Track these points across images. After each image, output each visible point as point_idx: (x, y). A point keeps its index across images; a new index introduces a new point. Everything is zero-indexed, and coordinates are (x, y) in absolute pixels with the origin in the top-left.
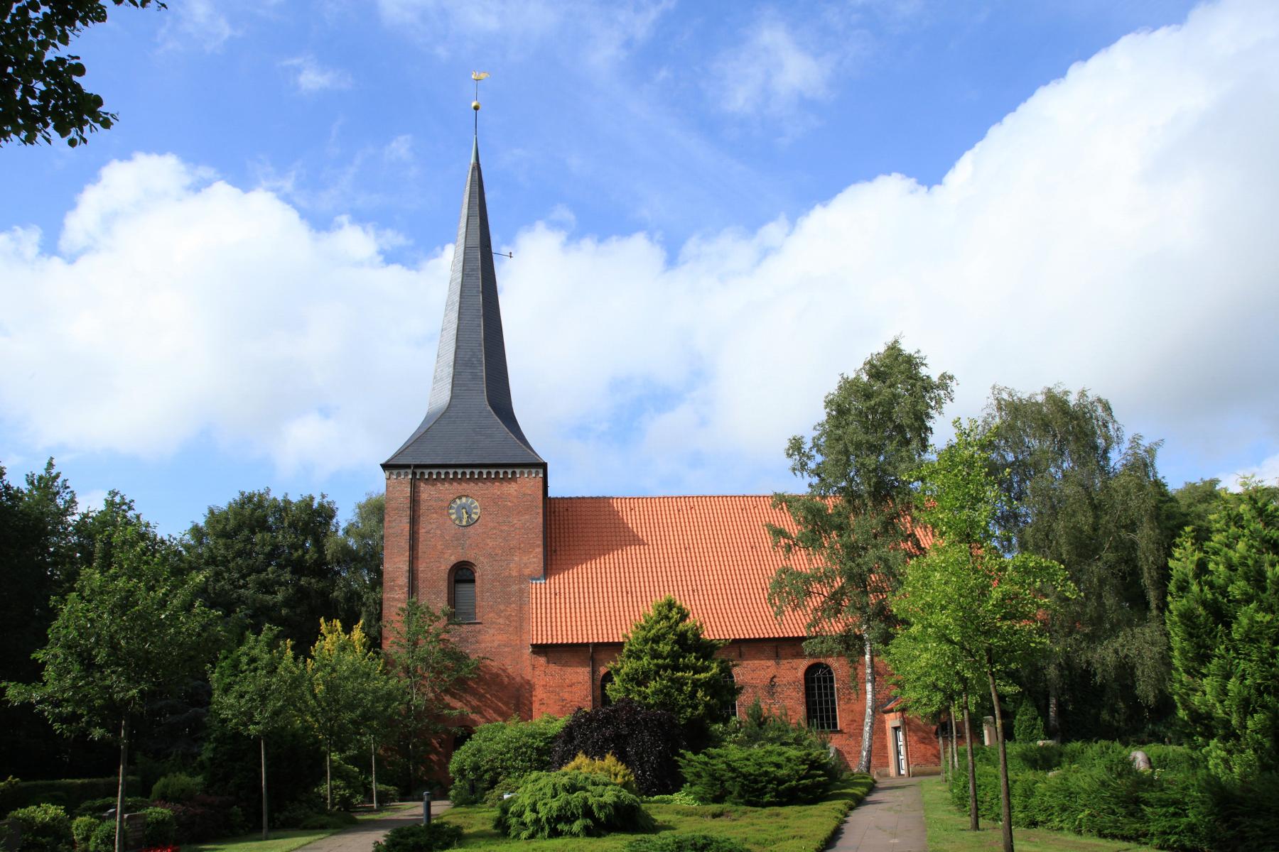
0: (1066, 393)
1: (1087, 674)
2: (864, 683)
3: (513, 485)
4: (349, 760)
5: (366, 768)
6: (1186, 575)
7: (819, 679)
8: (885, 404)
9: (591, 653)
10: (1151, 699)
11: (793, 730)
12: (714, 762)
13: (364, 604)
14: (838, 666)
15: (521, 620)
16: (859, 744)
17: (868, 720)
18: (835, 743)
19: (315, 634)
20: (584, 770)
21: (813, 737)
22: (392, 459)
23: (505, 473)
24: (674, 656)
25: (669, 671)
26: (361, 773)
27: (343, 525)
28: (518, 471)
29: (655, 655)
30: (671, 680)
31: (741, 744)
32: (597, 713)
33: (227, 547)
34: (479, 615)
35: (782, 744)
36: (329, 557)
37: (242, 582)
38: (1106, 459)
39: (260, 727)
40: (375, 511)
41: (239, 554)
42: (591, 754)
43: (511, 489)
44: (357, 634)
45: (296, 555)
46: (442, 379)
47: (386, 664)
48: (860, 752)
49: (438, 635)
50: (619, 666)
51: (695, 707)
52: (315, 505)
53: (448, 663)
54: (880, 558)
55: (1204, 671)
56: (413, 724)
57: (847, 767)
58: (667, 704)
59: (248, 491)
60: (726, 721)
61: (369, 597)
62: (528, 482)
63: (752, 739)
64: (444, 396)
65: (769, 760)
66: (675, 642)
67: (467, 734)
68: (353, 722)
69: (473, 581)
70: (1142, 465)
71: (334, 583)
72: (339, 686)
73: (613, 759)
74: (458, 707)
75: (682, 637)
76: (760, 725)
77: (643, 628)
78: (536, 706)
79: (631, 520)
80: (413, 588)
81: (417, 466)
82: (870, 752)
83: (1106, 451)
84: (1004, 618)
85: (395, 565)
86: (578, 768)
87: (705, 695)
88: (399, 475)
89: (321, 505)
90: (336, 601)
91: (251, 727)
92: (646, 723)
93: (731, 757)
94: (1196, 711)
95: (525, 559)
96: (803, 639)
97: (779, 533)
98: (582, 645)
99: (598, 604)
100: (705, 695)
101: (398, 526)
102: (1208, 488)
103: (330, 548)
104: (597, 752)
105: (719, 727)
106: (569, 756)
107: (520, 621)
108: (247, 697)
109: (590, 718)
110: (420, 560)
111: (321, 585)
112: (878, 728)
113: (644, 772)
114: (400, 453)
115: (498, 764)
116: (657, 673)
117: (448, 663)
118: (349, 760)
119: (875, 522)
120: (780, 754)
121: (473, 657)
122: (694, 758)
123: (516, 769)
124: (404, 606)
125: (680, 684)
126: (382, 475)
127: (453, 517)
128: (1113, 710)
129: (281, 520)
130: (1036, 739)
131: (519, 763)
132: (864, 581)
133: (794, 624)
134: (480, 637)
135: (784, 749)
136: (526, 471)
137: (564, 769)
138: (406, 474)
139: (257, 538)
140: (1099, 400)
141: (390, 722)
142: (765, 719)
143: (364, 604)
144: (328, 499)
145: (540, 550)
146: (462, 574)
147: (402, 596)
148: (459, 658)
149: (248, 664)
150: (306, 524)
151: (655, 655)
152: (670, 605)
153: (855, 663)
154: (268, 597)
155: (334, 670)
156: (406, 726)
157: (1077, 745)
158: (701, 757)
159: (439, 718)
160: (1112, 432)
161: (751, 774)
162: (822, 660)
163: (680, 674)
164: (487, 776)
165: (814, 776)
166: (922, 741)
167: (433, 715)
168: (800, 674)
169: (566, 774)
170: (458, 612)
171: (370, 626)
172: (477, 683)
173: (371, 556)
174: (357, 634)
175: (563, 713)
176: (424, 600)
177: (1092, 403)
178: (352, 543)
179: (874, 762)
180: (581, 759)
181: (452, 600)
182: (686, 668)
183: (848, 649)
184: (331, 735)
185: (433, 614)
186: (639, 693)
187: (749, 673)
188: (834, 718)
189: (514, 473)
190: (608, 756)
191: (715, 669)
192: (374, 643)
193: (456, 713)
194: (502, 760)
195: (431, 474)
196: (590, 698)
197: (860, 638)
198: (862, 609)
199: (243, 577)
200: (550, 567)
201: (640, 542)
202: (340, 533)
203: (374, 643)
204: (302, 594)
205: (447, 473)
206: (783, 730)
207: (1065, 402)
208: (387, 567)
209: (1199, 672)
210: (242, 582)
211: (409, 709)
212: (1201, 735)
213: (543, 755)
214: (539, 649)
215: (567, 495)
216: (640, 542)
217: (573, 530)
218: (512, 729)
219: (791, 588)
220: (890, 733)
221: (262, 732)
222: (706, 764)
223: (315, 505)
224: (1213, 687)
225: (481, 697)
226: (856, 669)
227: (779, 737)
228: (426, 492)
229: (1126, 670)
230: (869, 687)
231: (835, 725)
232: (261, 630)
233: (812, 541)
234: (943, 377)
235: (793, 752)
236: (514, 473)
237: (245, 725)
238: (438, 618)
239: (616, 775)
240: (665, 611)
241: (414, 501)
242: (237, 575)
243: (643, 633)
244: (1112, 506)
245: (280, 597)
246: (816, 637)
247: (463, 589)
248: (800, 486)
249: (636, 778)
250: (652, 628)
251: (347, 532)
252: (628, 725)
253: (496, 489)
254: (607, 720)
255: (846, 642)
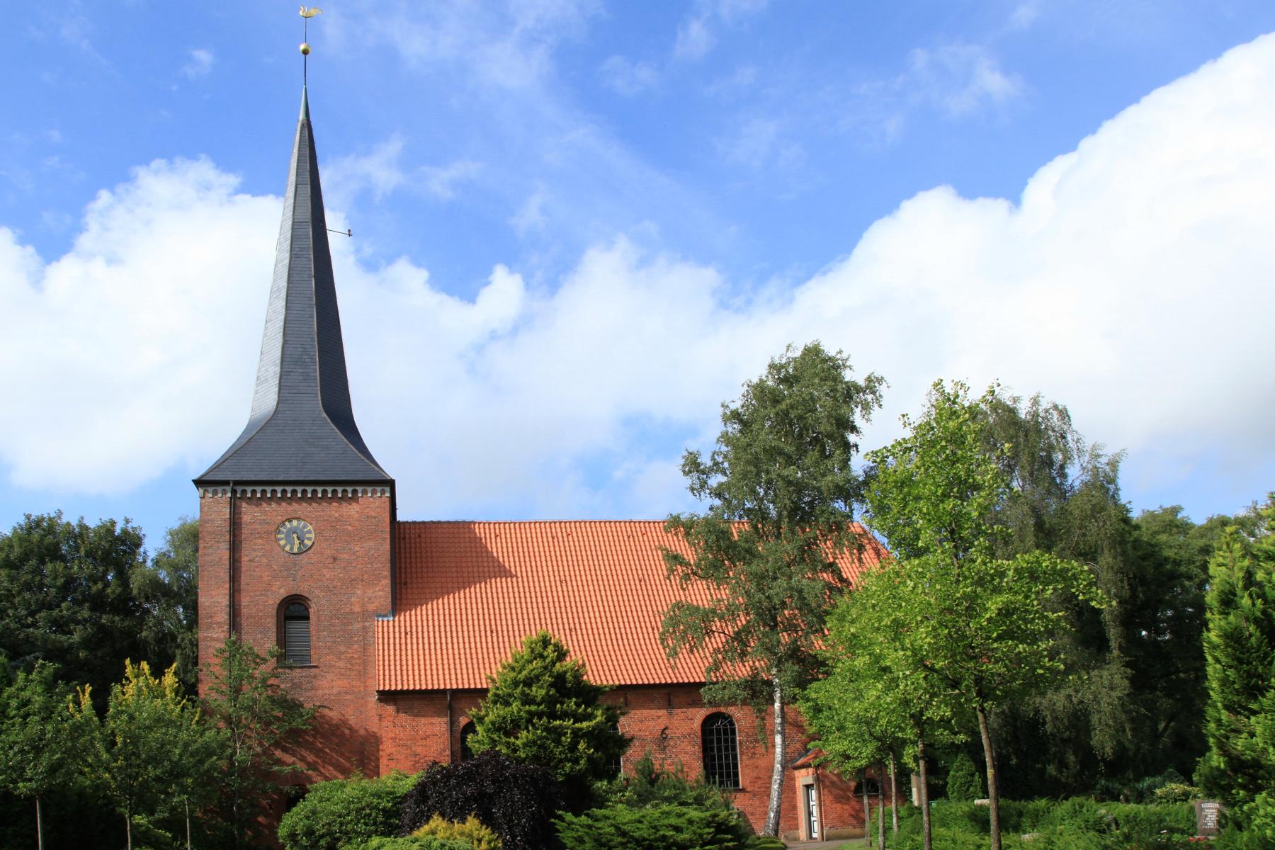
0: (1015, 400)
1: (1036, 723)
2: (773, 734)
3: (355, 506)
4: (160, 824)
5: (179, 833)
6: (1232, 585)
7: (718, 731)
8: (801, 413)
9: (447, 701)
10: (1108, 750)
11: (692, 788)
12: (599, 825)
13: (178, 646)
14: (742, 717)
15: (365, 664)
16: (765, 805)
17: (776, 777)
18: (739, 803)
19: (120, 677)
20: (440, 835)
21: (716, 795)
22: (206, 474)
23: (345, 491)
24: (550, 701)
25: (545, 719)
26: (175, 838)
27: (152, 554)
28: (360, 489)
29: (527, 700)
30: (547, 729)
31: (629, 803)
32: (456, 767)
33: (12, 579)
34: (314, 657)
35: (681, 804)
36: (135, 592)
37: (30, 620)
38: (1064, 476)
39: (34, 785)
40: (189, 537)
41: (28, 587)
42: (448, 816)
43: (352, 510)
44: (169, 679)
45: (94, 589)
46: (266, 380)
47: (204, 713)
48: (766, 813)
49: (264, 681)
50: (483, 713)
51: (576, 761)
52: (118, 531)
53: (278, 713)
54: (792, 589)
55: (1254, 707)
56: (235, 782)
57: (752, 831)
58: (542, 757)
59: (36, 513)
60: (612, 776)
61: (183, 637)
62: (373, 502)
63: (642, 799)
64: (270, 400)
65: (666, 822)
66: (552, 685)
67: (301, 795)
68: (158, 779)
69: (307, 618)
70: (1103, 485)
71: (142, 620)
72: (139, 737)
73: (476, 822)
74: (290, 763)
75: (559, 680)
76: (652, 782)
77: (513, 669)
78: (383, 762)
79: (497, 549)
80: (234, 622)
81: (237, 483)
82: (778, 813)
83: (1062, 467)
84: (1000, 638)
85: (213, 599)
86: (433, 833)
87: (588, 748)
88: (215, 493)
89: (125, 531)
90: (145, 641)
91: (21, 785)
92: (516, 779)
93: (619, 819)
94: (1238, 758)
95: (369, 593)
96: (702, 685)
97: (675, 559)
98: (438, 691)
99: (462, 643)
100: (588, 748)
101: (216, 553)
102: (1168, 518)
103: (136, 583)
104: (456, 813)
105: (602, 785)
106: (421, 818)
107: (363, 666)
108: (16, 749)
109: (447, 774)
110: (243, 594)
111: (126, 623)
112: (787, 786)
113: (514, 837)
114: (218, 466)
115: (336, 828)
116: (529, 721)
117: (278, 713)
118: (160, 824)
119: (788, 548)
120: (679, 816)
121: (308, 706)
122: (575, 820)
123: (359, 834)
124: (223, 646)
125: (557, 734)
126: (196, 493)
127: (282, 543)
128: (1062, 764)
129: (77, 549)
130: (973, 798)
131: (361, 827)
132: (774, 618)
133: (691, 668)
134: (316, 683)
135: (684, 809)
136: (369, 489)
137: (416, 834)
138: (224, 492)
139: (48, 568)
140: (1055, 407)
141: (207, 780)
142: (658, 776)
143: (178, 646)
144: (134, 524)
145: (387, 582)
146: (293, 610)
147: (222, 636)
148: (291, 707)
149: (18, 708)
150: (107, 553)
151: (527, 700)
152: (545, 642)
153: (762, 709)
154: (64, 638)
155: (132, 718)
156: (228, 785)
157: (1042, 803)
158: (583, 819)
159: (269, 775)
160: (1071, 444)
161: (645, 839)
162: (723, 709)
163: (558, 722)
164: (323, 842)
165: (721, 841)
166: (839, 799)
167: (261, 772)
168: (697, 724)
169: (416, 840)
170: (290, 652)
171: (186, 672)
172: (314, 736)
173: (187, 591)
174: (169, 679)
175: (414, 768)
176: (248, 640)
177: (1047, 411)
178: (164, 576)
179: (782, 825)
180: (436, 822)
181: (282, 640)
182: (564, 715)
183: (753, 697)
184: (131, 795)
185: (258, 656)
186: (508, 745)
187: (638, 723)
188: (736, 775)
189: (355, 492)
190: (469, 818)
191: (600, 717)
192: (188, 689)
193: (287, 769)
194: (341, 824)
195: (254, 492)
196: (448, 752)
197: (769, 683)
198: (770, 650)
199: (32, 614)
200: (400, 600)
201: (507, 574)
202: (149, 564)
203: (188, 689)
204: (102, 636)
205: (274, 492)
206: (680, 787)
207: (1012, 411)
208: (203, 600)
209: (1246, 708)
210: (30, 620)
211: (232, 764)
212: (1243, 787)
213: (391, 817)
214: (387, 696)
215: (419, 519)
216: (507, 574)
217: (426, 560)
218: (354, 788)
219: (687, 625)
220: (800, 792)
221: (36, 790)
222: (590, 827)
223: (118, 531)
224: (1265, 727)
225: (318, 752)
226: (763, 719)
227: (675, 797)
228: (249, 514)
229: (1079, 720)
230: (778, 739)
231: (736, 783)
232: (33, 667)
233: (712, 571)
234: (869, 380)
235: (694, 813)
236: (355, 492)
237: (15, 782)
238: (265, 660)
239: (480, 841)
240: (539, 649)
241: (235, 524)
242: (24, 612)
243: (513, 675)
244: (1068, 531)
245: (76, 637)
246: (717, 683)
247: (295, 627)
248: (702, 507)
249: (505, 844)
250: (523, 668)
251: (157, 563)
252: (493, 782)
253: (334, 510)
254: (469, 776)
255: (751, 688)
